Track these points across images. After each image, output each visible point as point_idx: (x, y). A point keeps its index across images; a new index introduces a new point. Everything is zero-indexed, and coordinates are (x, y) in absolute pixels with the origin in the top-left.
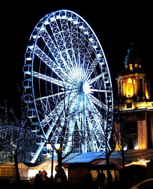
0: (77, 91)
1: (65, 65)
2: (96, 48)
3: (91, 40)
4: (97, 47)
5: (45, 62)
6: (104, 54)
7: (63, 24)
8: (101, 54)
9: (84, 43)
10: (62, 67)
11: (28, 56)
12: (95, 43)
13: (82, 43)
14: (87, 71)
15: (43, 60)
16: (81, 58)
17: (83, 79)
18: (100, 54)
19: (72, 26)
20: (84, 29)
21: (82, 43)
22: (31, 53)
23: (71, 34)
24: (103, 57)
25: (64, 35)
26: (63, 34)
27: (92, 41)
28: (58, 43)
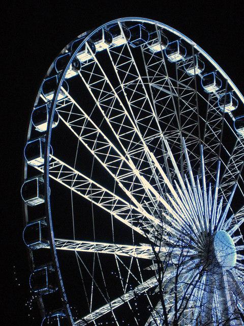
3: (211, 89)
22: (40, 182)
23: (147, 86)
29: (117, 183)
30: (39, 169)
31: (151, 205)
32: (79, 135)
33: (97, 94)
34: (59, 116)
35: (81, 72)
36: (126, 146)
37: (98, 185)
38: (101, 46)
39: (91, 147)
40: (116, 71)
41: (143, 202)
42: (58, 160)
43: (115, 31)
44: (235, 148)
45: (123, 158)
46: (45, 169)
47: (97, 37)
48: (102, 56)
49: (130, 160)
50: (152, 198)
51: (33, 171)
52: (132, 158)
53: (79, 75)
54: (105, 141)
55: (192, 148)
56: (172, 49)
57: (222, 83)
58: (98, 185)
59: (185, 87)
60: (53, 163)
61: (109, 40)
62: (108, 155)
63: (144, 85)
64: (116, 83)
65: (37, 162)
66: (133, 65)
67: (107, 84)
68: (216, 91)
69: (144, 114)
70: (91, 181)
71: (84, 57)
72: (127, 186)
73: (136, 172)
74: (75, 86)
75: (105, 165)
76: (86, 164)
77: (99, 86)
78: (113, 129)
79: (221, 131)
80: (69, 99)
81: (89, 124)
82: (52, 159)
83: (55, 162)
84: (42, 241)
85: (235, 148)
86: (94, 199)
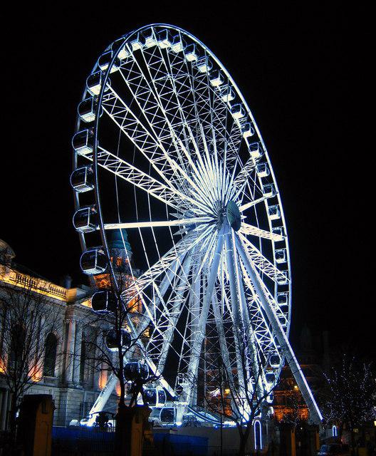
0: (211, 223)
2: (230, 102)
3: (216, 82)
5: (128, 179)
8: (260, 151)
9: (205, 98)
12: (224, 88)
13: (201, 100)
14: (231, 184)
15: (122, 177)
16: (207, 140)
17: (225, 195)
21: (201, 100)
22: (88, 172)
28: (150, 117)
31: (178, 182)
33: (134, 88)
34: (103, 108)
36: (158, 133)
37: (139, 171)
38: (137, 45)
40: (149, 69)
42: (105, 151)
43: (148, 33)
47: (134, 38)
48: (137, 53)
51: (82, 160)
56: (189, 50)
57: (225, 80)
58: (139, 171)
62: (125, 118)
64: (149, 80)
65: (84, 151)
68: (220, 85)
71: (123, 55)
72: (160, 167)
73: (166, 155)
74: (116, 80)
75: (132, 139)
76: (128, 153)
81: (130, 116)
84: (87, 184)
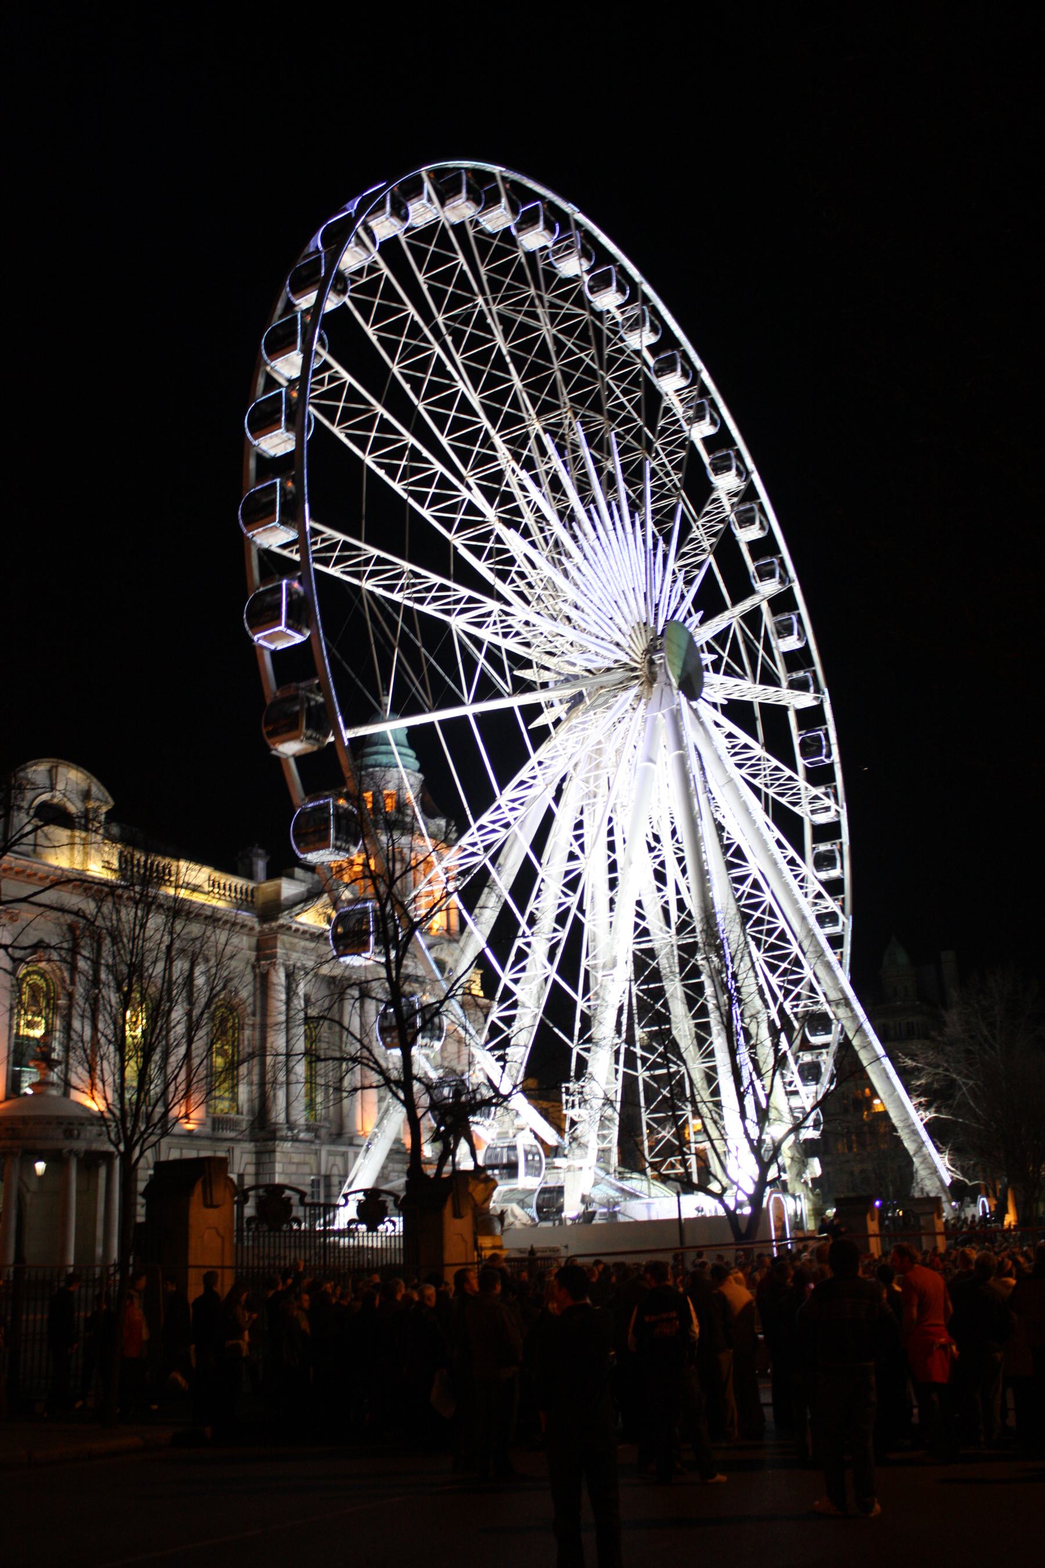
1: (520, 560)
4: (652, 339)
6: (756, 478)
7: (653, 1112)
8: (739, 474)
10: (489, 495)
11: (265, 423)
18: (734, 472)
19: (482, 263)
20: (550, 244)
24: (750, 494)
25: (457, 345)
26: (449, 339)
27: (613, 310)
29: (455, 548)
30: (285, 553)
32: (364, 451)
35: (350, 297)
38: (385, 227)
39: (393, 478)
40: (425, 288)
41: (513, 581)
42: (337, 367)
44: (661, 423)
45: (465, 494)
46: (303, 551)
48: (390, 249)
49: (475, 490)
50: (533, 572)
52: (478, 485)
53: (344, 304)
54: (426, 461)
55: (593, 439)
59: (562, 308)
60: (327, 374)
61: (400, 212)
63: (624, 1073)
64: (428, 316)
66: (462, 272)
67: (414, 323)
68: (619, 307)
69: (493, 381)
70: (407, 566)
77: (397, 328)
78: (468, 812)
79: (639, 394)
80: (336, 372)
82: (325, 362)
83: (324, 536)
85: (661, 423)
86: (411, 494)
